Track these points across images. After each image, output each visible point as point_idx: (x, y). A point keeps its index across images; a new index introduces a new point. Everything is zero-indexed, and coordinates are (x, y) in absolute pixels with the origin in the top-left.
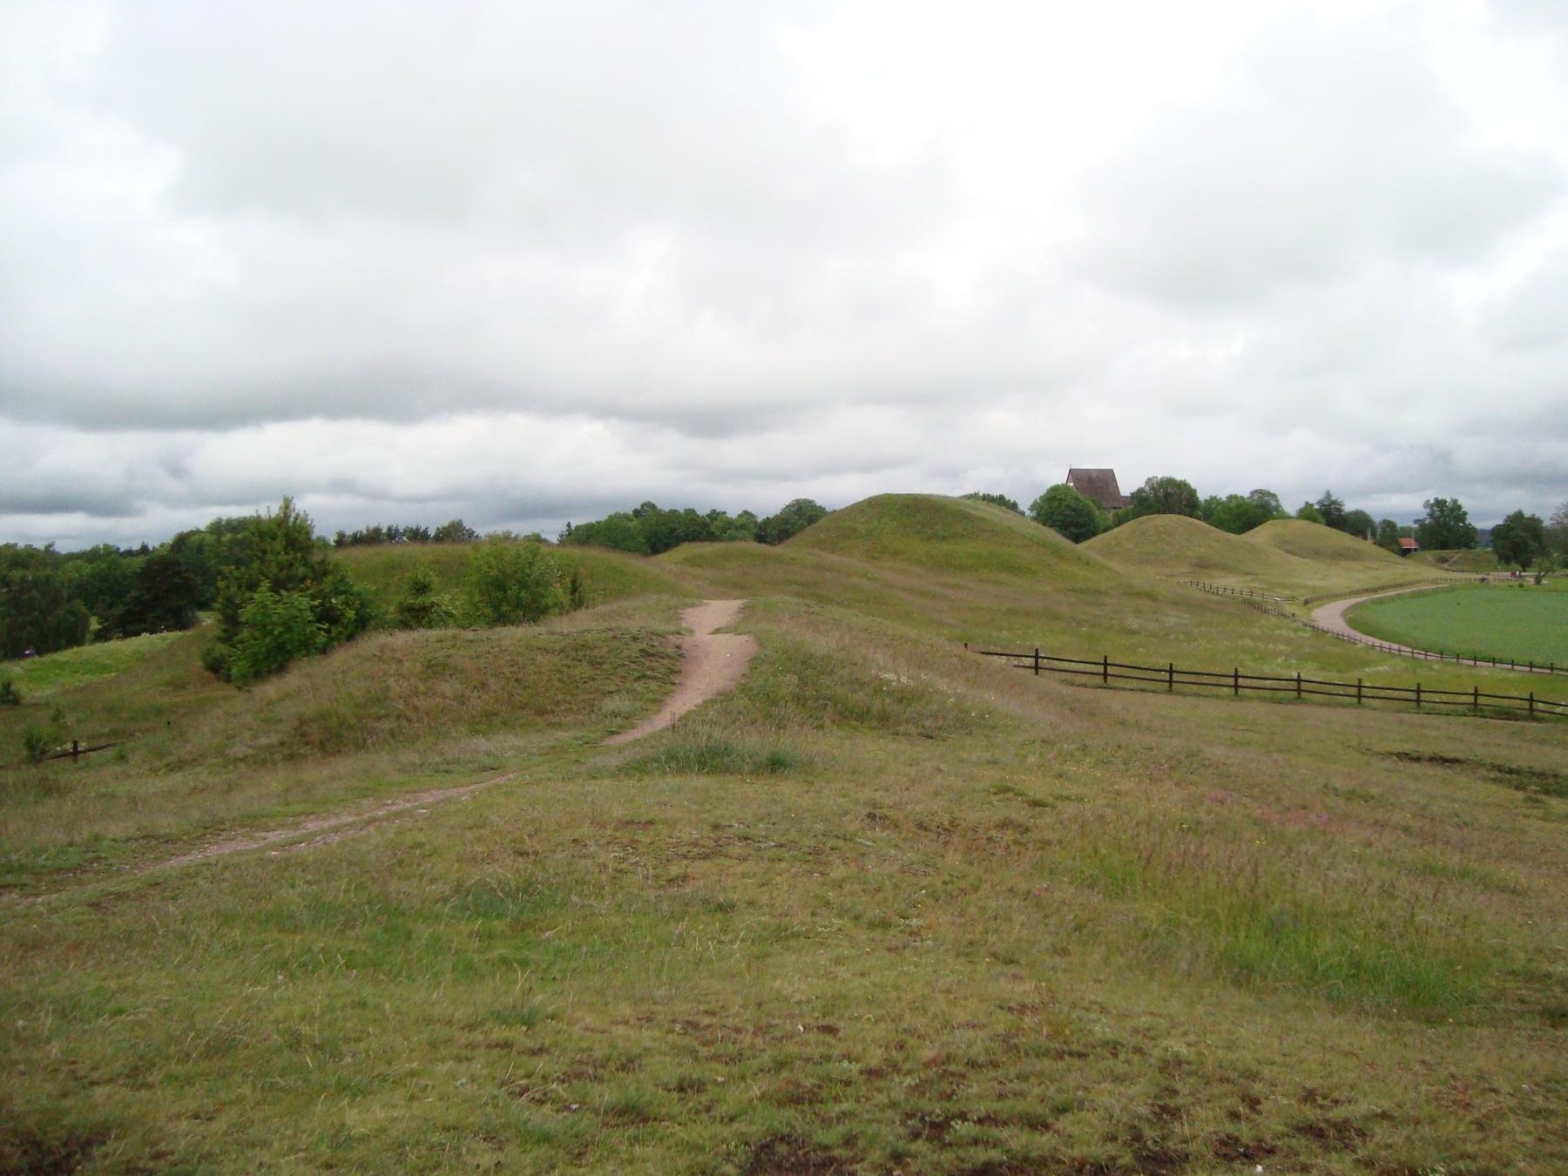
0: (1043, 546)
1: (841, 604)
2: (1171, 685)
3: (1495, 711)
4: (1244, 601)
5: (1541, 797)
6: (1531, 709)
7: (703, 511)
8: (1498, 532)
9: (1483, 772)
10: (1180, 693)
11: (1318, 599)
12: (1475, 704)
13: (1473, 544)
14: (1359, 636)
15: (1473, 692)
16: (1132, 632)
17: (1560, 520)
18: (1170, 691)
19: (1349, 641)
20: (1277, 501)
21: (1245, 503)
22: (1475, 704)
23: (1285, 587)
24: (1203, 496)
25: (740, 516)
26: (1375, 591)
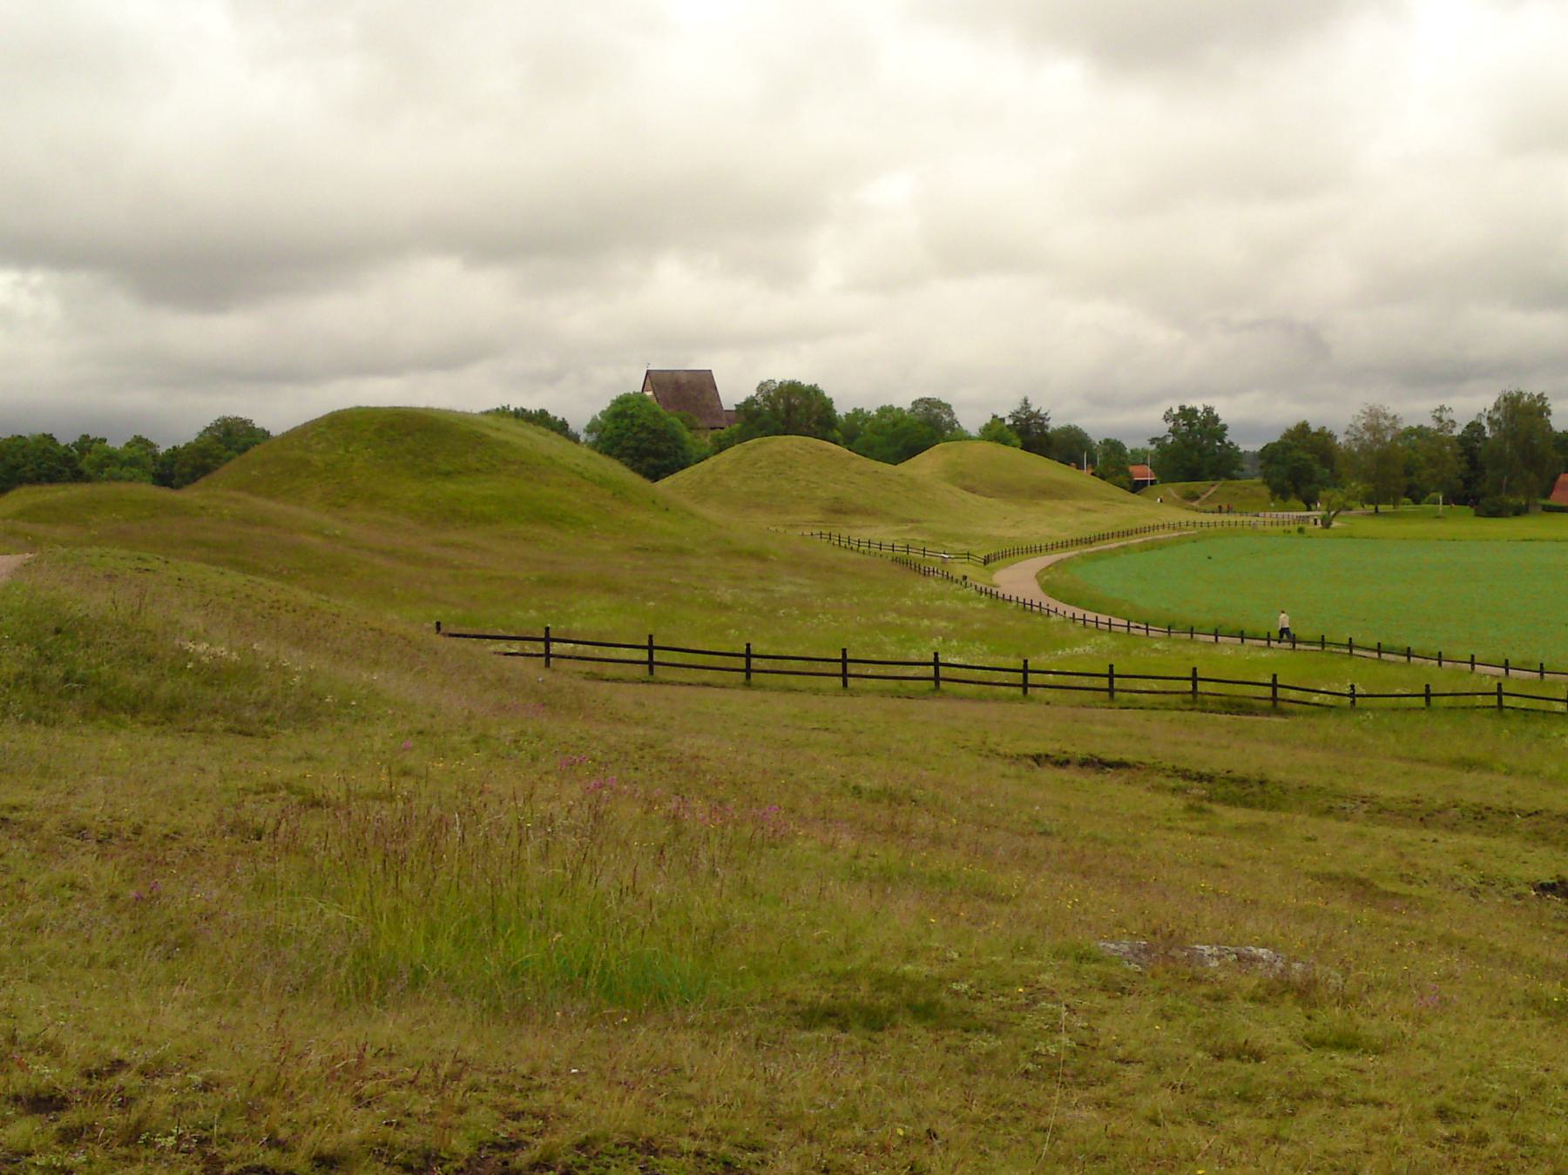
0: (601, 485)
1: (272, 575)
2: (748, 677)
3: (1222, 703)
4: (896, 560)
5: (1206, 805)
6: (1274, 698)
7: (66, 438)
8: (1272, 456)
9: (1159, 779)
10: (761, 687)
11: (1005, 555)
12: (1194, 692)
13: (1235, 472)
14: (1053, 604)
15: (1189, 675)
16: (724, 607)
17: (1359, 435)
18: (748, 685)
19: (1040, 613)
20: (951, 414)
21: (903, 418)
22: (1194, 692)
23: (958, 538)
24: (842, 409)
25: (128, 444)
26: (1089, 541)
